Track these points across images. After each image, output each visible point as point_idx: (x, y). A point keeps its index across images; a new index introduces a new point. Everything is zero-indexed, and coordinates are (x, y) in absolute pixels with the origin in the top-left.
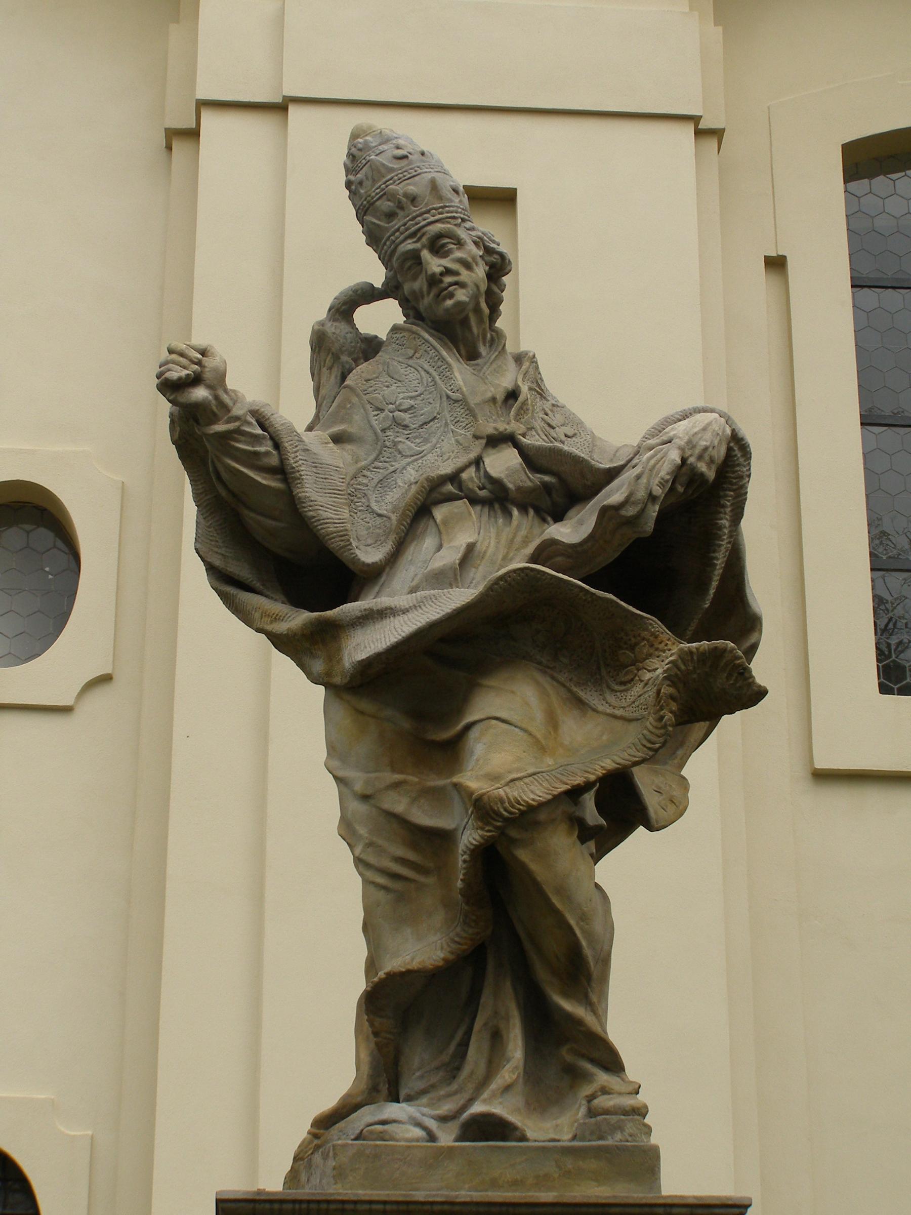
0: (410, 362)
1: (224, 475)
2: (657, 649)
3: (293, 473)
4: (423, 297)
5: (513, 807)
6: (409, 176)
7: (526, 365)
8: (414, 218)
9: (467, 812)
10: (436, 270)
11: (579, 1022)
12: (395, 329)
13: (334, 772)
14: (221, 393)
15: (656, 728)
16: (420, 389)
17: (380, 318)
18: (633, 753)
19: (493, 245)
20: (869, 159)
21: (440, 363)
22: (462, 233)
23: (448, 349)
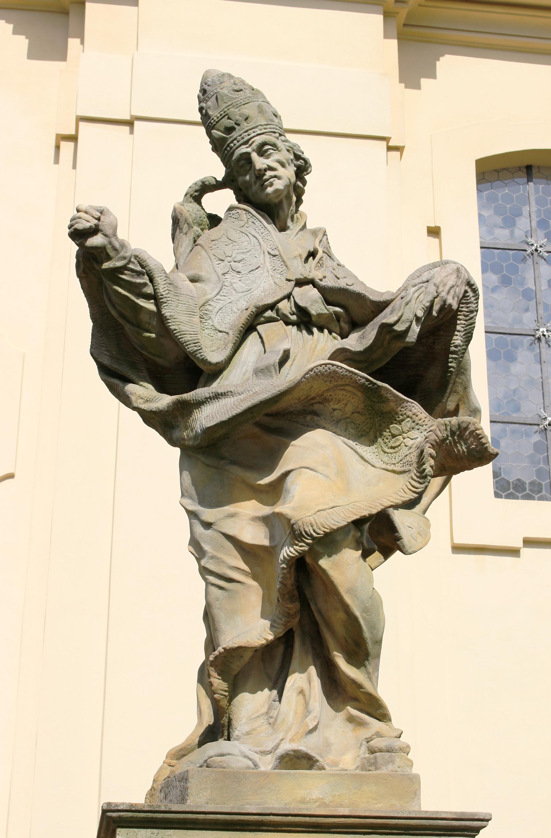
0: (243, 229)
1: (114, 298)
2: (417, 424)
3: (162, 299)
4: (251, 186)
5: (320, 529)
6: (243, 103)
7: (320, 236)
8: (247, 131)
9: (286, 532)
10: (255, 178)
11: (359, 686)
12: (231, 209)
13: (187, 507)
14: (113, 240)
15: (418, 477)
16: (249, 248)
17: (221, 201)
18: (402, 495)
19: (300, 153)
20: (495, 172)
21: (263, 230)
22: (279, 143)
23: (269, 223)
